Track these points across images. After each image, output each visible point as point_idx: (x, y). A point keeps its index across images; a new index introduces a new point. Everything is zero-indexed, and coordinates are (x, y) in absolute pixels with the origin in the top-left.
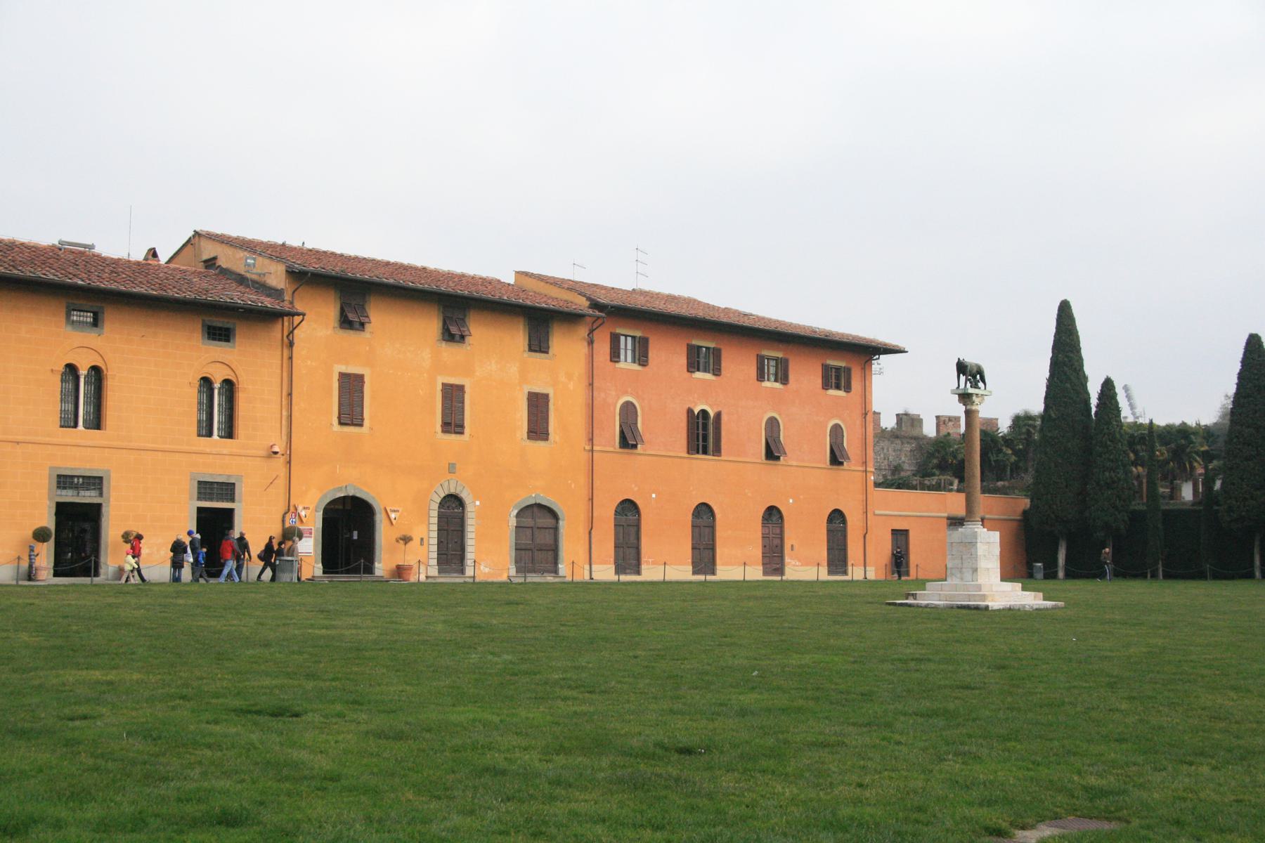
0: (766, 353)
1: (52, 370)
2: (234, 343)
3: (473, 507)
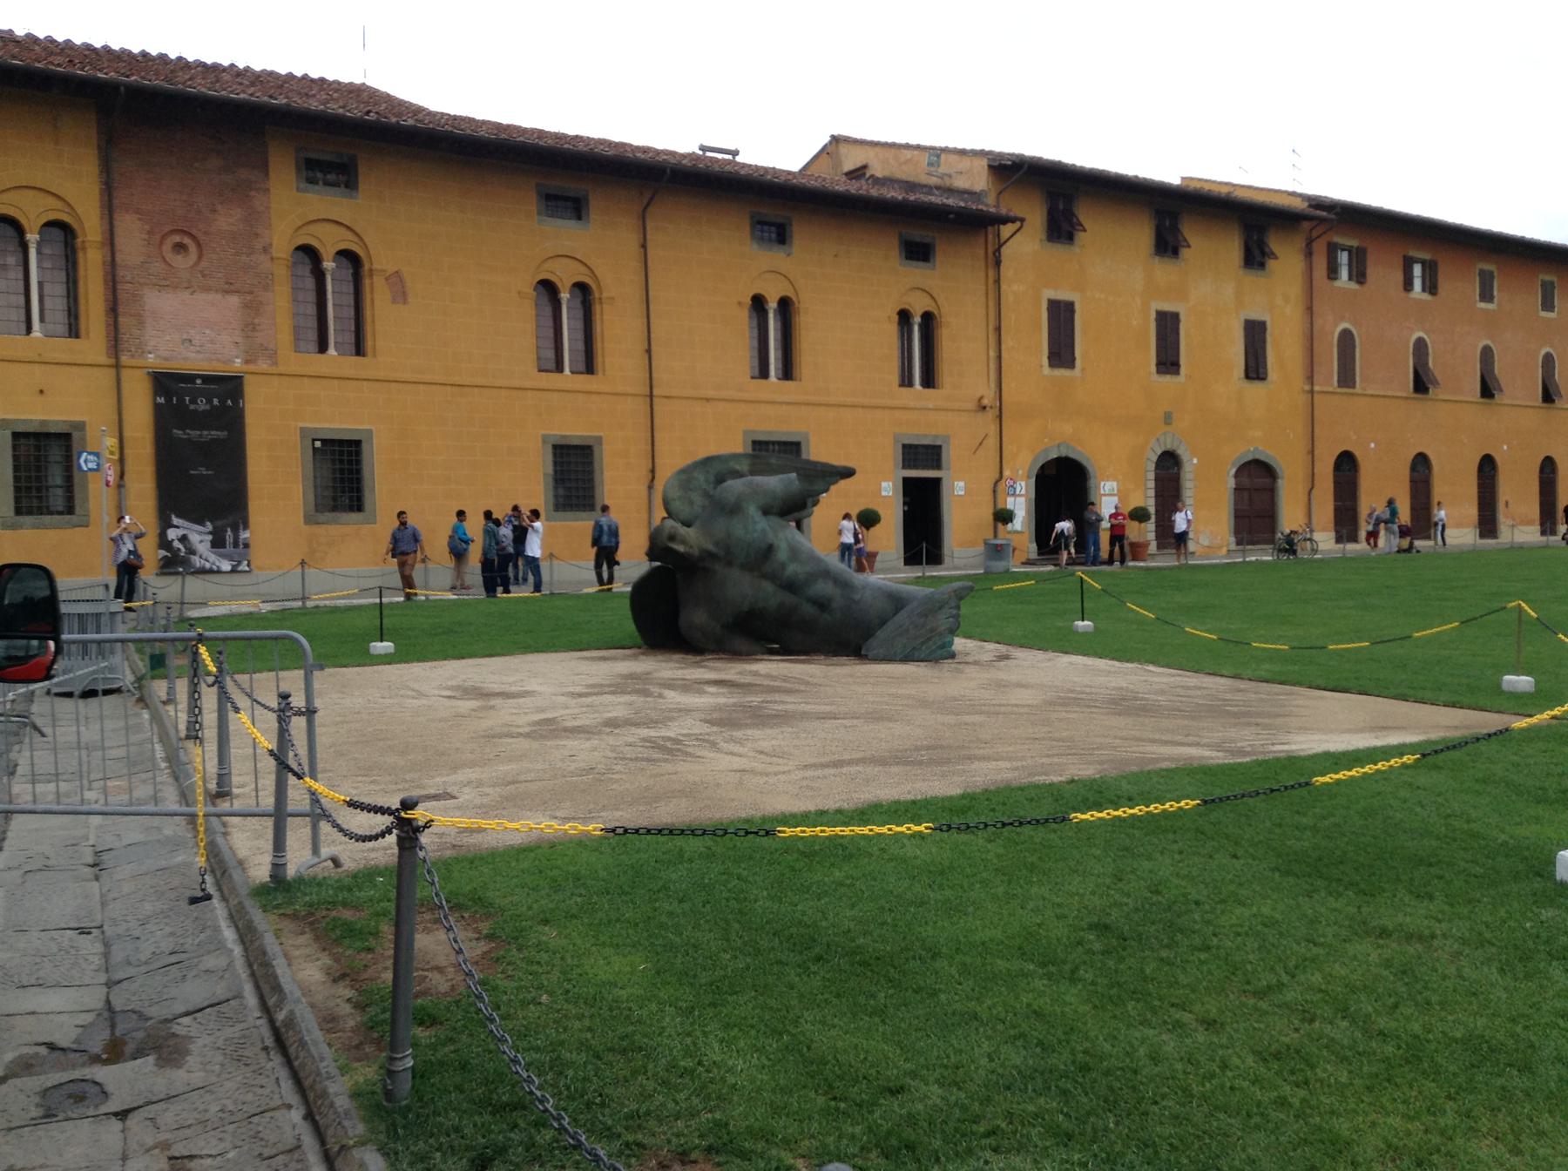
0: (1339, 239)
3: (1191, 464)
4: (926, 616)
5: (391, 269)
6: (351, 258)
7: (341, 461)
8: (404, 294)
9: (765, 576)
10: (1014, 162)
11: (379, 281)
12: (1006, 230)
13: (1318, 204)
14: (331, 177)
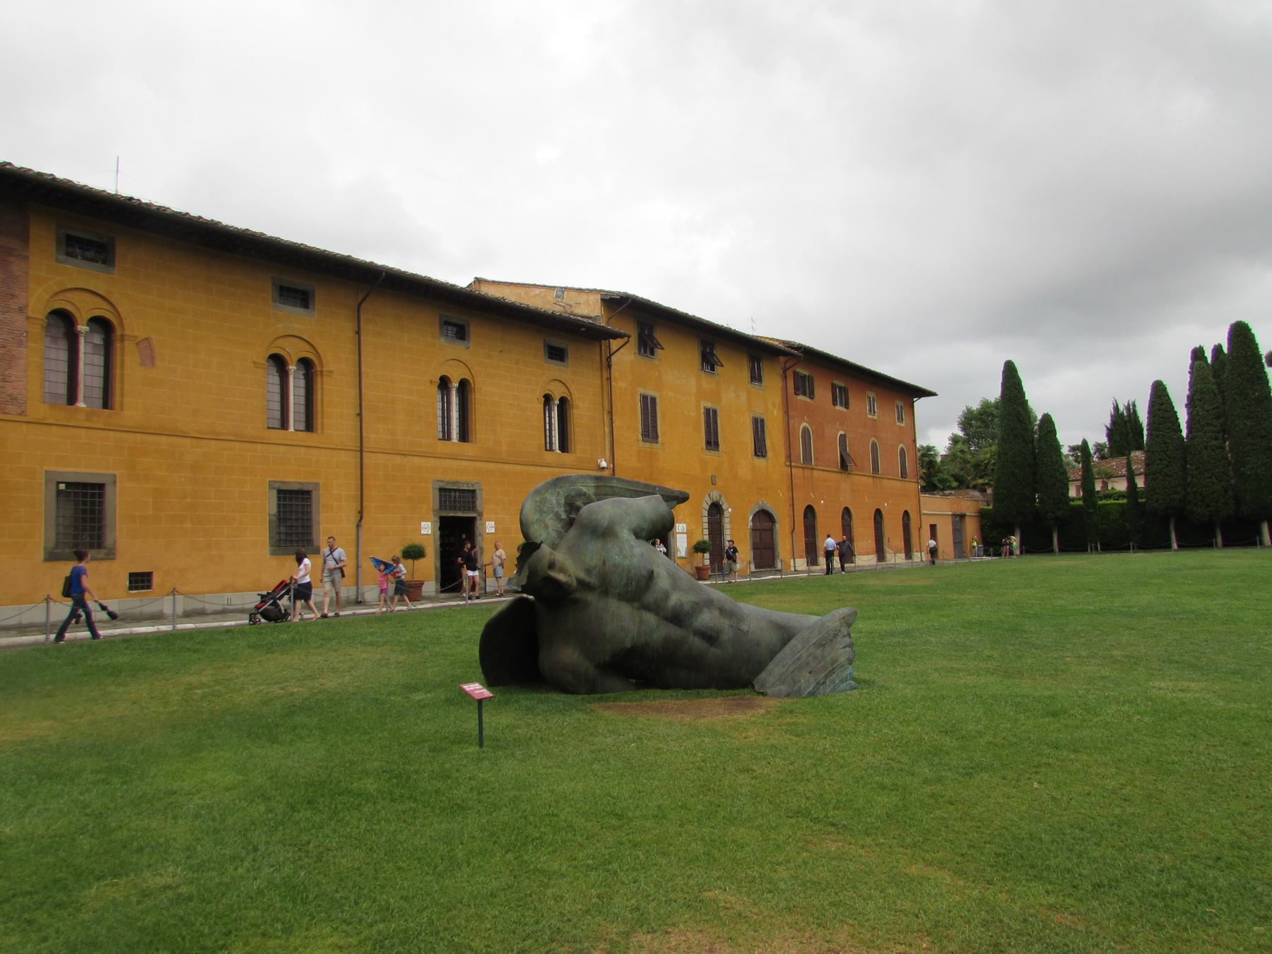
1: (431, 382)
2: (314, 310)
3: (728, 511)
4: (824, 646)
5: (142, 335)
6: (102, 325)
7: (84, 503)
8: (153, 358)
9: (647, 608)
10: (622, 297)
11: (129, 346)
12: (615, 344)
13: (791, 346)
14: (90, 254)
